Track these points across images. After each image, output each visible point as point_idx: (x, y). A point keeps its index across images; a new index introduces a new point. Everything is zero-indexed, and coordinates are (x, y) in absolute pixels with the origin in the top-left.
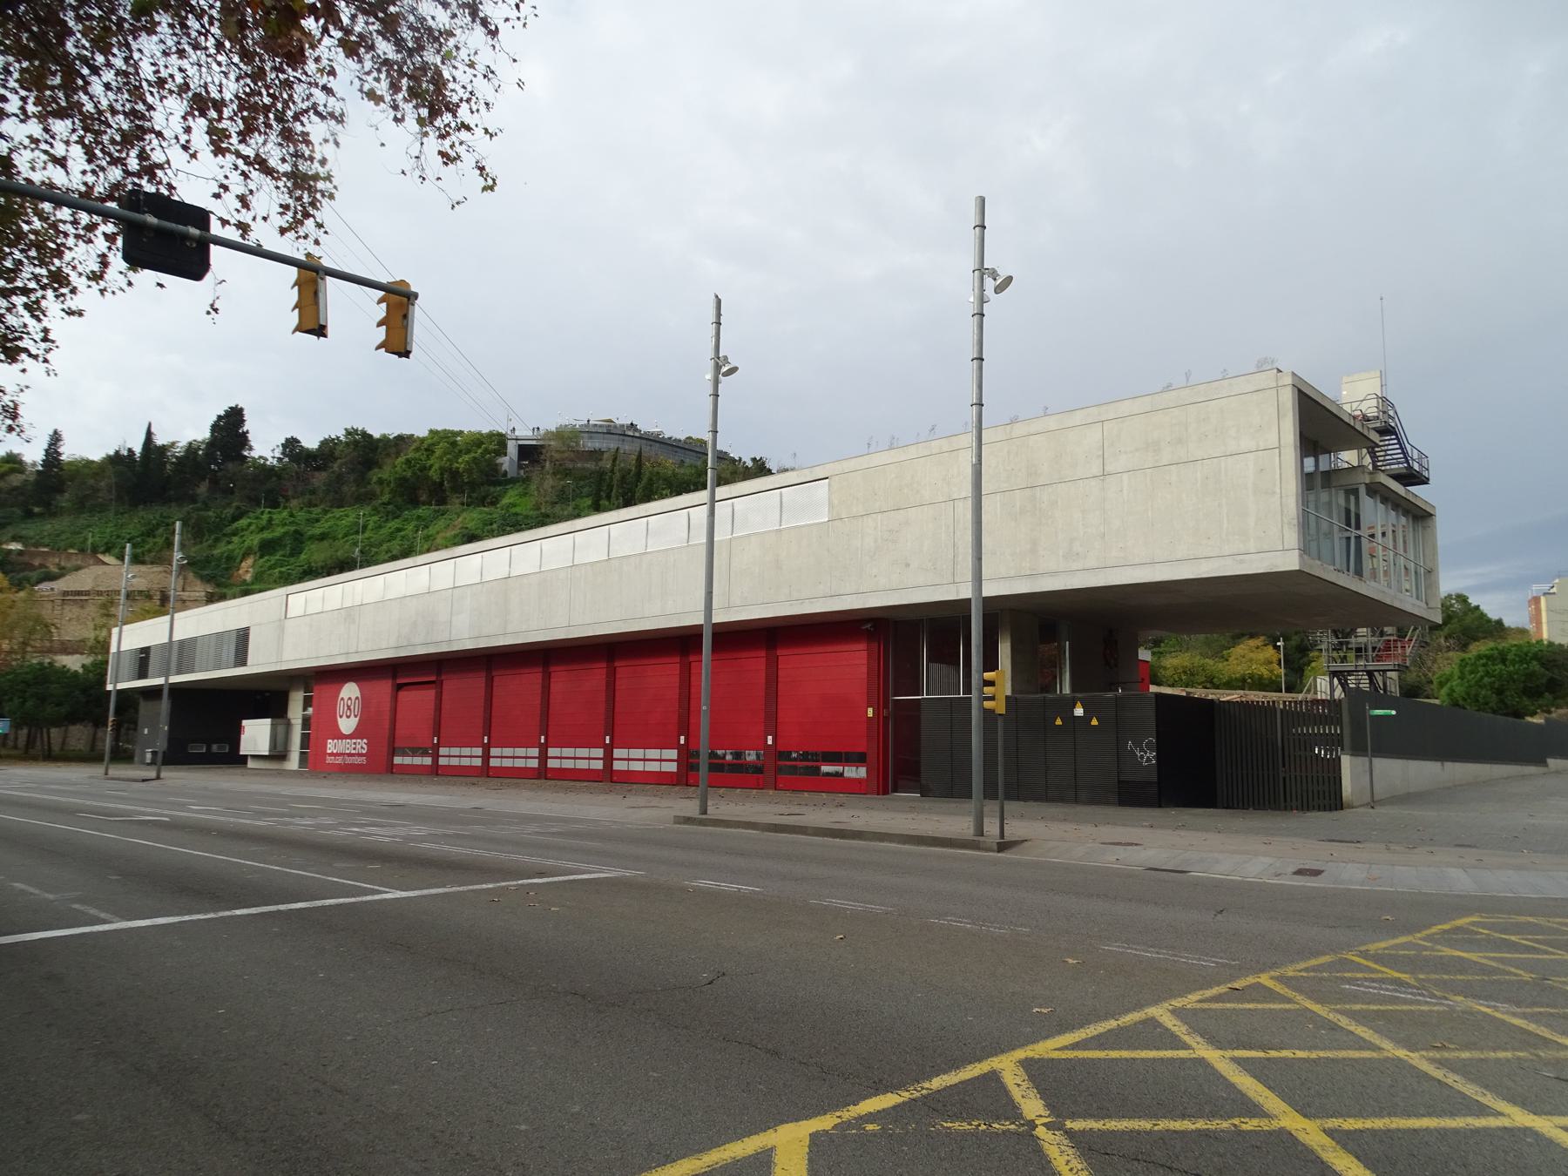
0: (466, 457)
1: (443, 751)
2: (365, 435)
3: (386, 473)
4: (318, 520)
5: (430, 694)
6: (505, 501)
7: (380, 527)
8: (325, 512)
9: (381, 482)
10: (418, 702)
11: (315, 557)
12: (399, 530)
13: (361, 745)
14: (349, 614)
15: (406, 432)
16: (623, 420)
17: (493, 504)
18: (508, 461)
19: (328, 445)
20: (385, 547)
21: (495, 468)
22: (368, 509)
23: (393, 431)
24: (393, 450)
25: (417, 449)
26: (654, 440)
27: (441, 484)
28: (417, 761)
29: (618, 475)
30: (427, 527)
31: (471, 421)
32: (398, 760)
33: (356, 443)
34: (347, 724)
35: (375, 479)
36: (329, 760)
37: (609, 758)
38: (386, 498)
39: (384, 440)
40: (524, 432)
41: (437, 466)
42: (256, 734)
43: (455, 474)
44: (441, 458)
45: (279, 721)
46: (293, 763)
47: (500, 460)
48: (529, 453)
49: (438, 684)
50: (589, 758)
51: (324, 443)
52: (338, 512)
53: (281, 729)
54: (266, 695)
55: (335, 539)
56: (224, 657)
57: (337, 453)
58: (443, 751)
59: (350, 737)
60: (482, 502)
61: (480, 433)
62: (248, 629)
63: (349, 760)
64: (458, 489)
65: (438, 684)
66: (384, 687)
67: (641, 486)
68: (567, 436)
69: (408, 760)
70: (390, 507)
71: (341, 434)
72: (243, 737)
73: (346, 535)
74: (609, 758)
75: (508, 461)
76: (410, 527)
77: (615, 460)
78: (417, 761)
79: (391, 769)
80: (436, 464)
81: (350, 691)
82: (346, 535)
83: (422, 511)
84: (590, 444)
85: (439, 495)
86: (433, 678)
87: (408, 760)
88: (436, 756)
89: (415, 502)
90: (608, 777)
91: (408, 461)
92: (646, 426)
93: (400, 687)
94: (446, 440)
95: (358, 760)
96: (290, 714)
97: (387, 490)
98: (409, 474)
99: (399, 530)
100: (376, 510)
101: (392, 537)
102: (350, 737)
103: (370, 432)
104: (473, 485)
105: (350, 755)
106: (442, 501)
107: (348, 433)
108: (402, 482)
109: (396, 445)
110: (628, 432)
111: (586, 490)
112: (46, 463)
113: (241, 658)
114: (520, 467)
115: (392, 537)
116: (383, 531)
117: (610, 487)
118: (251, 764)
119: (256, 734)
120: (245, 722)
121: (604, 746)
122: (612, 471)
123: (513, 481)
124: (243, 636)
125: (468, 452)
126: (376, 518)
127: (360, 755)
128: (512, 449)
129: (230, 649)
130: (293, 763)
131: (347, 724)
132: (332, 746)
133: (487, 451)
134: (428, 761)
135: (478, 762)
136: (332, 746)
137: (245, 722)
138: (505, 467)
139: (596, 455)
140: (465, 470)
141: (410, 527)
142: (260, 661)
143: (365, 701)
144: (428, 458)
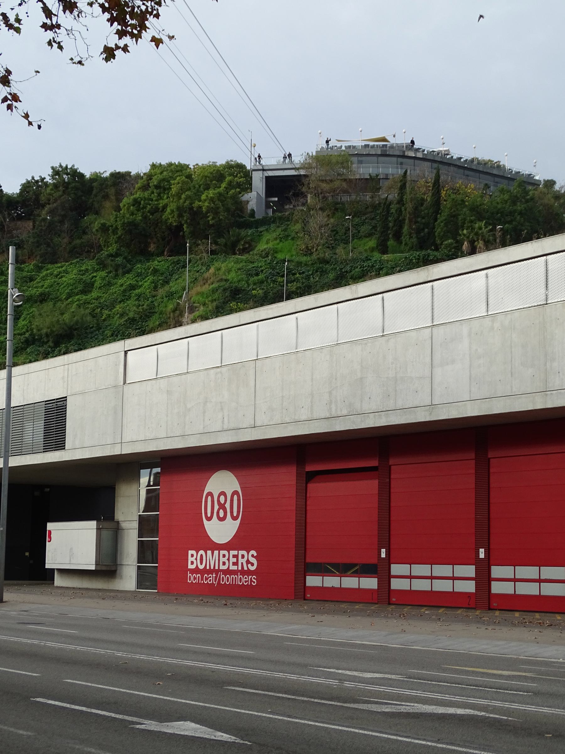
0: (211, 193)
1: (396, 569)
2: (75, 174)
3: (108, 217)
4: (31, 279)
5: (369, 487)
6: (262, 246)
7: (109, 284)
8: (39, 269)
9: (104, 229)
10: (347, 498)
11: (37, 322)
12: (133, 287)
13: (248, 559)
14: (233, 371)
15: (122, 169)
16: (400, 139)
17: (245, 251)
18: (254, 198)
19: (32, 189)
20: (118, 308)
21: (240, 206)
22: (89, 264)
23: (106, 168)
24: (112, 191)
25: (145, 187)
26: (440, 162)
27: (180, 227)
28: (350, 582)
29: (409, 206)
30: (167, 282)
31: (202, 151)
32: (313, 581)
33: (66, 185)
34: (221, 530)
35: (96, 226)
36: (191, 578)
37: (484, 579)
38: (113, 249)
39: (96, 178)
40: (272, 159)
41: (172, 206)
42: (71, 543)
43: (195, 214)
44: (178, 195)
45: (107, 524)
46: (128, 580)
47: (245, 197)
48: (283, 187)
49: (382, 473)
50: (460, 578)
51: (27, 187)
52: (55, 269)
53: (106, 534)
54: (87, 489)
55: (57, 300)
56: (28, 438)
57: (43, 198)
58: (396, 569)
59: (228, 547)
60: (231, 249)
61: (214, 165)
62: (64, 399)
63: (226, 580)
64: (199, 234)
65: (382, 473)
66: (285, 478)
67: (442, 218)
68: (332, 161)
69: (332, 582)
70: (119, 260)
71: (46, 174)
72: (49, 546)
73: (69, 296)
74: (484, 579)
75: (254, 198)
76: (147, 283)
77: (403, 187)
78: (350, 582)
79: (302, 595)
80: (170, 207)
81: (223, 484)
82: (69, 296)
83: (158, 263)
84: (365, 170)
85: (174, 242)
86: (374, 463)
87: (332, 582)
88: (385, 578)
89: (145, 254)
90: (484, 602)
91: (136, 202)
92: (428, 143)
93: (311, 477)
94: (166, 177)
95: (244, 580)
96: (119, 516)
97: (113, 239)
98: (139, 218)
99: (133, 287)
100: (102, 265)
101: (125, 295)
102: (228, 547)
103: (81, 170)
104: (219, 230)
105: (228, 572)
106: (178, 250)
107: (56, 172)
108: (131, 227)
109: (115, 184)
110: (406, 154)
111: (365, 229)
112: (114, 22)
113: (55, 436)
114: (268, 206)
115: (125, 295)
116: (113, 289)
117: (400, 223)
118: (58, 581)
119: (71, 543)
120: (50, 526)
121: (477, 562)
122: (401, 201)
123: (265, 221)
124: (55, 414)
125: (207, 188)
126: (103, 274)
127: (243, 572)
128: (258, 182)
129: (35, 430)
130: (128, 580)
131: (221, 530)
132: (194, 559)
133: (231, 185)
134: (370, 583)
135: (470, 587)
136: (194, 559)
137: (50, 526)
138: (252, 205)
139: (372, 183)
140: (209, 210)
141: (147, 283)
142: (85, 442)
143: (249, 497)
144: (160, 197)
